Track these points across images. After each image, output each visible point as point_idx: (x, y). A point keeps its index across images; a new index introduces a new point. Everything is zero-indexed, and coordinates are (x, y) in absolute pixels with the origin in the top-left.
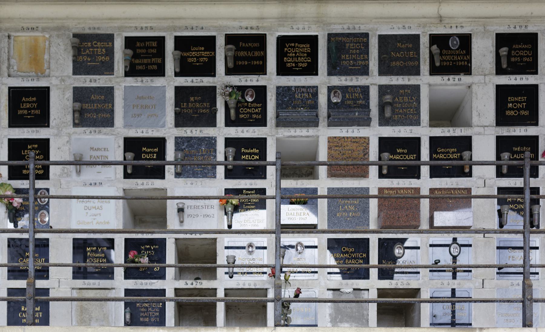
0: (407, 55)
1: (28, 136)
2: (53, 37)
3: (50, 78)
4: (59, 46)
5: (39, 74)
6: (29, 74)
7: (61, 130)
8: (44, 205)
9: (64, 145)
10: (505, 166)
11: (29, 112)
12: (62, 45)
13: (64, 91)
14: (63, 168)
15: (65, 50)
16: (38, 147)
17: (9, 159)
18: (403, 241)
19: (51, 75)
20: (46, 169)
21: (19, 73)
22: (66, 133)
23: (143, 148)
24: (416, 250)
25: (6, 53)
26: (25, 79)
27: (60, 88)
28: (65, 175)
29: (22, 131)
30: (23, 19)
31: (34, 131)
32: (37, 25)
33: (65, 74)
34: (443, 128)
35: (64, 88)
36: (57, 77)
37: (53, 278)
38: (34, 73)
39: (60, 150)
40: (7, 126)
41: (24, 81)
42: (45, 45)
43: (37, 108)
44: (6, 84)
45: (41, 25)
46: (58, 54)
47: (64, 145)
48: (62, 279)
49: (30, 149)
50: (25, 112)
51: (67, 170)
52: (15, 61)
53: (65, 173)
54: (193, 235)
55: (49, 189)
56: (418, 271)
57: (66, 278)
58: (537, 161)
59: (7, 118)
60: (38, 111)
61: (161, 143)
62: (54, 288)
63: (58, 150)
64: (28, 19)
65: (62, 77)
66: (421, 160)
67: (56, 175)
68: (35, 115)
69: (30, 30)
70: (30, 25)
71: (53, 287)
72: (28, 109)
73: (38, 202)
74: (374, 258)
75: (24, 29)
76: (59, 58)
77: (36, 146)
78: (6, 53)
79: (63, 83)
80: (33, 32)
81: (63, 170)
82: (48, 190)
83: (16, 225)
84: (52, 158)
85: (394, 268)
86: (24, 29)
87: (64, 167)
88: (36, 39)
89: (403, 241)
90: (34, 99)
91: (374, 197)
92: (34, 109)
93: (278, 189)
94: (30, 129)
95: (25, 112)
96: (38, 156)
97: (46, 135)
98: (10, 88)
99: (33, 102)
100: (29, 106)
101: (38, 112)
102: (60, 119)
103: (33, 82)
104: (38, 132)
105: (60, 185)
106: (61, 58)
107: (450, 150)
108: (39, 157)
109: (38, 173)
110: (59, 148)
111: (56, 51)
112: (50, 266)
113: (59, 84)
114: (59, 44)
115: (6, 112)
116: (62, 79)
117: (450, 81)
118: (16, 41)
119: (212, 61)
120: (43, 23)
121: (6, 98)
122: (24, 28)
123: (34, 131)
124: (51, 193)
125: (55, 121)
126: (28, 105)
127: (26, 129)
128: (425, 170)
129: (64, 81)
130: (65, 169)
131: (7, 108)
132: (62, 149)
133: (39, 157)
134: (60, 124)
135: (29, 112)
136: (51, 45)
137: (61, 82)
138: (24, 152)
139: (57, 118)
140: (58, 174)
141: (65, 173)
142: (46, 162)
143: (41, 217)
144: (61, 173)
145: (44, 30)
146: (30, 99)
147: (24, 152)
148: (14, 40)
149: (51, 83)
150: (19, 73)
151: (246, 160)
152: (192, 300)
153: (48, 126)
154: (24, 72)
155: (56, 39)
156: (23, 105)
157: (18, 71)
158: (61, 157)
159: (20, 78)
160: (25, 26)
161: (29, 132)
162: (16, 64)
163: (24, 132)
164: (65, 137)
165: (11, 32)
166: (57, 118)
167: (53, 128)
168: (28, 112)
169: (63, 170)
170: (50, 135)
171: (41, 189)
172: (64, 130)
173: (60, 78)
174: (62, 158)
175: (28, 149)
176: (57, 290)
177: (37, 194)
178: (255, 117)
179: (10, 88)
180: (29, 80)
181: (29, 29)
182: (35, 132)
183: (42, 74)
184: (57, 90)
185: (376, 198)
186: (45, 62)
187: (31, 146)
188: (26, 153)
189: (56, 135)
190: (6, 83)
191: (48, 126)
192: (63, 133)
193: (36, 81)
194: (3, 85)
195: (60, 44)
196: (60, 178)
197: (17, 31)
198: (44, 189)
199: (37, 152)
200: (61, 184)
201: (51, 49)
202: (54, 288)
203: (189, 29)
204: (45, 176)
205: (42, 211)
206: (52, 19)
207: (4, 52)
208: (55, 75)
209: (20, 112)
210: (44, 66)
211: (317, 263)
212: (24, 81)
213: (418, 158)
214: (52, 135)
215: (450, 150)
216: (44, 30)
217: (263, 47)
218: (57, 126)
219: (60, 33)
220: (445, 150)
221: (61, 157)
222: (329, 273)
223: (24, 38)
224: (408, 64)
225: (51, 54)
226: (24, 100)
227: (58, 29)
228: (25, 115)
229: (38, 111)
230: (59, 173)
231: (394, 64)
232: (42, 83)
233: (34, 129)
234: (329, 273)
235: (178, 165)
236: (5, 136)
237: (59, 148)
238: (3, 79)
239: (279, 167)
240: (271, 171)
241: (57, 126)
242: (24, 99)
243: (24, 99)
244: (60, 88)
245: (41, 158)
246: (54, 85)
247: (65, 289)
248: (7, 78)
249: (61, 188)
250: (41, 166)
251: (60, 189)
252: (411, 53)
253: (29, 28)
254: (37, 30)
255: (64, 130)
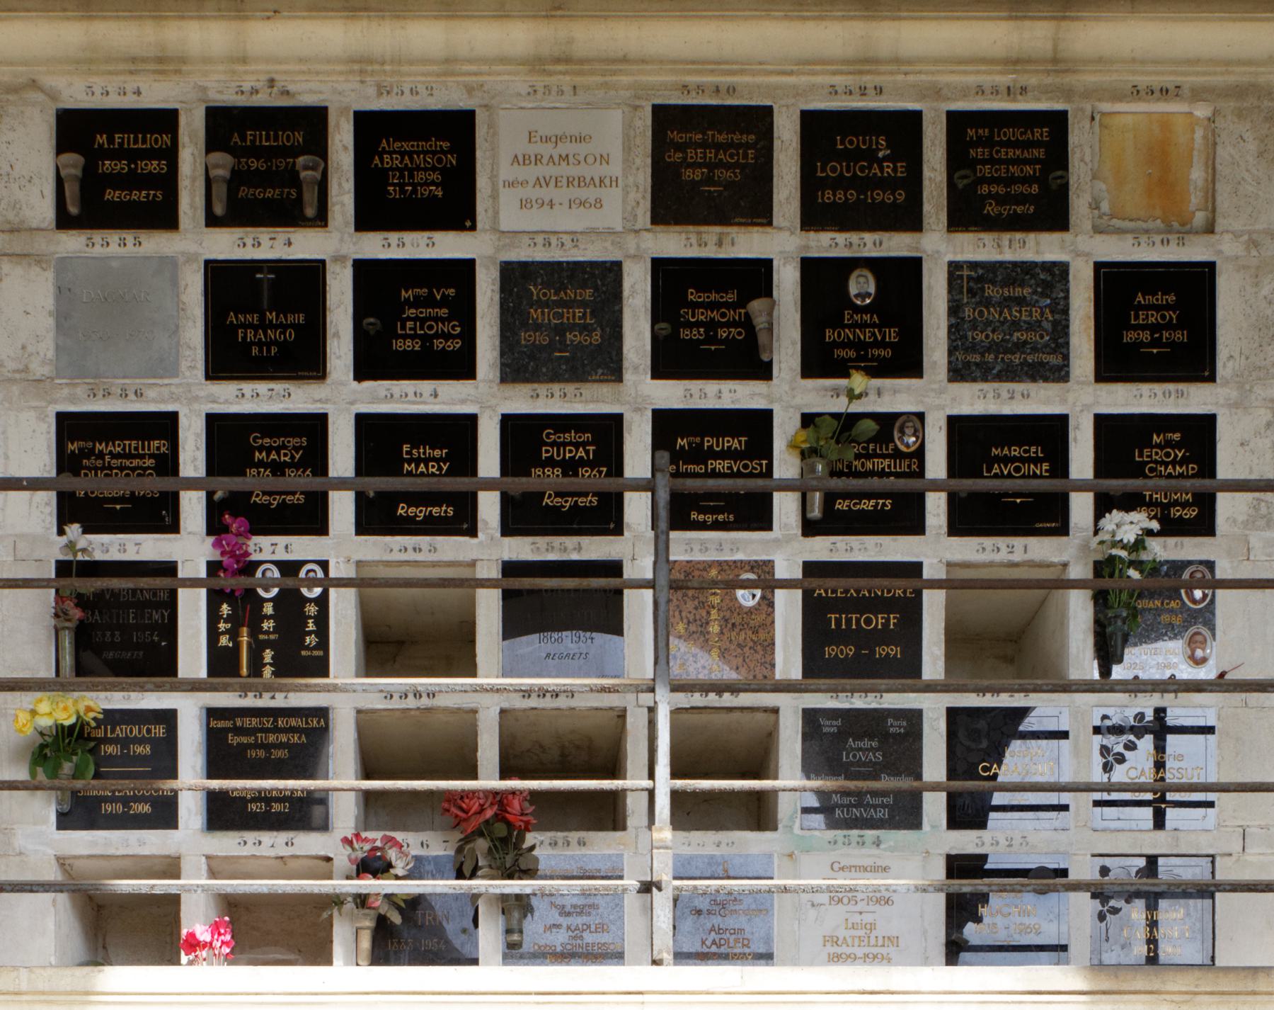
0: (848, 171)
1: (1153, 406)
2: (1225, 116)
3: (1217, 237)
4: (1242, 143)
5: (1175, 224)
6: (1144, 225)
7: (1250, 391)
8: (1201, 609)
9: (1257, 433)
10: (818, 494)
11: (1156, 335)
12: (1251, 140)
13: (1257, 276)
14: (1255, 502)
15: (1260, 155)
16: (1181, 437)
17: (1098, 473)
18: (1023, 712)
19: (1218, 228)
20: (1206, 503)
21: (1116, 223)
22: (1265, 400)
23: (679, 440)
24: (1201, 738)
25: (1086, 164)
26: (1143, 239)
27: (1245, 267)
28: (1262, 523)
29: (1135, 393)
30: (1143, 62)
31: (1170, 393)
32: (1179, 79)
33: (1259, 227)
34: (536, 386)
35: (1258, 268)
36: (1237, 235)
37: (1227, 823)
38: (1159, 221)
39: (1247, 448)
40: (1092, 378)
41: (1139, 244)
42: (1193, 139)
43: (1180, 326)
44: (1088, 255)
45: (1188, 80)
46: (1238, 165)
47: (1257, 433)
48: (1253, 826)
49: (1158, 446)
50: (1145, 336)
51: (1268, 508)
52: (1104, 187)
53: (1263, 517)
54: (267, 695)
55: (1214, 562)
56: (1063, 802)
57: (1263, 823)
58: (474, 479)
59: (1092, 355)
60: (1183, 335)
61: (166, 425)
62: (1231, 855)
63: (1240, 449)
64: (1155, 62)
65: (1250, 233)
66: (182, 474)
67: (1235, 521)
68: (1172, 344)
69: (1157, 94)
70: (1156, 81)
71: (1227, 850)
72: (1154, 328)
73: (1182, 600)
74: (934, 764)
75: (1138, 91)
76: (1243, 179)
77: (1176, 436)
78: (1086, 164)
79: (1254, 253)
80: (1166, 100)
81: (1257, 508)
82: (1210, 565)
83: (1105, 671)
84: (1224, 470)
85: (990, 794)
86: (1138, 91)
87: (1258, 499)
88: (1165, 122)
89: (1023, 712)
90: (1171, 298)
91: (935, 584)
92: (1169, 326)
93: (663, 565)
94: (1158, 388)
95: (1145, 336)
96: (1181, 467)
97: (1205, 404)
98: (1098, 266)
99: (1168, 307)
100: (1156, 319)
101: (1181, 336)
102: (1247, 358)
103: (1166, 249)
104: (1182, 395)
105: (1245, 550)
106: (1246, 175)
107: (289, 442)
108: (1184, 468)
109: (1181, 515)
110: (1242, 444)
111: (1232, 156)
112: (1170, 791)
113: (1244, 253)
114: (1241, 137)
115: (1090, 336)
116: (1250, 239)
117: (292, 247)
118: (1106, 127)
119: (169, 183)
120: (1197, 74)
121: (1087, 295)
122: (1139, 88)
123: (1170, 393)
124: (1219, 575)
125: (1230, 364)
126: (1153, 315)
127: (1145, 388)
128: (342, 507)
129: (1256, 244)
130: (1263, 504)
131: (1092, 323)
132: (1252, 445)
133: (1184, 468)
134: (1246, 373)
135: (1156, 335)
136: (1218, 140)
137: (1248, 249)
138: (1141, 455)
139: (1236, 355)
140: (1241, 518)
141: (1263, 517)
142: (1203, 484)
143: (1194, 646)
144: (1249, 515)
145: (1198, 94)
146: (1160, 299)
147: (1141, 455)
148: (1101, 125)
149: (1220, 252)
150: (1116, 223)
151: (724, 476)
152: (228, 885)
153: (1212, 378)
154: (1131, 220)
155: (1234, 123)
156: (1137, 317)
157: (1112, 216)
158: (1251, 468)
159: (1130, 236)
160: (1143, 80)
161: (1155, 394)
162: (1106, 194)
163: (1141, 396)
164: (1262, 411)
165: (1099, 100)
166: (1236, 355)
167: (1226, 383)
168: (1152, 335)
169: (1257, 508)
170: (1217, 403)
171: (1190, 563)
172: (1258, 390)
173: (1246, 237)
174: (1251, 472)
175: (1152, 447)
176: (1238, 860)
177: (1181, 576)
178: (441, 346)
179: (1098, 266)
180: (1154, 243)
181: (1153, 93)
182: (1173, 396)
183: (1183, 225)
184: (1238, 271)
185: (940, 587)
186: (1192, 188)
187: (1162, 436)
188: (1148, 456)
189: (1236, 405)
190: (1087, 250)
191: (1212, 378)
192: (1257, 399)
193: (1175, 246)
194: (1078, 255)
195: (1245, 137)
196: (1248, 532)
197: (1117, 96)
198: (1201, 562)
199: (1180, 455)
200: (1248, 549)
201: (1219, 150)
202: (1231, 855)
203: (1142, 93)
204: (1204, 525)
205: (1192, 630)
206: (1228, 63)
207: (1082, 160)
208: (1230, 228)
209: (1129, 337)
210: (1190, 202)
211: (1212, 779)
212: (1139, 244)
213: (617, 468)
214: (1223, 406)
215: (289, 442)
216: (1198, 94)
217: (318, 143)
218: (1238, 379)
219: (1245, 105)
220: (275, 442)
221: (1251, 468)
222: (1097, 804)
223: (1129, 119)
224: (872, 198)
225: (1218, 167)
226: (1139, 302)
227: (1239, 92)
228: (1142, 344)
229: (1183, 335)
230: (1245, 518)
231: (829, 198)
232: (1193, 252)
233: (1171, 387)
234: (1097, 804)
235: (817, 490)
236: (1086, 407)
237: (1242, 444)
238: (1079, 238)
239: (664, 496)
240: (637, 508)
241: (1238, 379)
242: (1141, 299)
243: (1140, 298)
244: (1245, 267)
245: (1190, 472)
246: (1227, 258)
247: (1262, 857)
248: (1091, 237)
249: (1248, 559)
250: (1190, 495)
251: (1245, 562)
252: (899, 165)
253: (1154, 88)
254: (1177, 95)
255: (1258, 390)
